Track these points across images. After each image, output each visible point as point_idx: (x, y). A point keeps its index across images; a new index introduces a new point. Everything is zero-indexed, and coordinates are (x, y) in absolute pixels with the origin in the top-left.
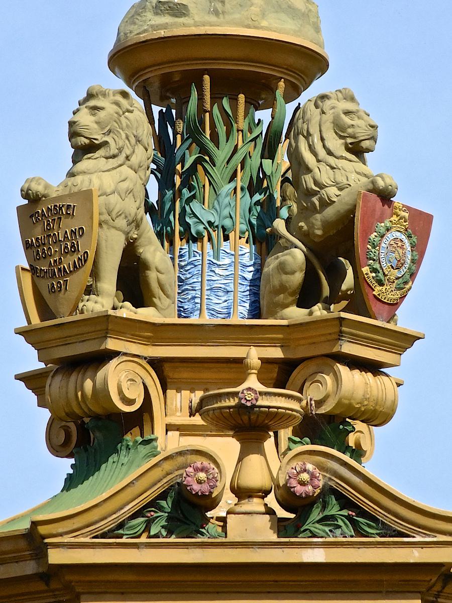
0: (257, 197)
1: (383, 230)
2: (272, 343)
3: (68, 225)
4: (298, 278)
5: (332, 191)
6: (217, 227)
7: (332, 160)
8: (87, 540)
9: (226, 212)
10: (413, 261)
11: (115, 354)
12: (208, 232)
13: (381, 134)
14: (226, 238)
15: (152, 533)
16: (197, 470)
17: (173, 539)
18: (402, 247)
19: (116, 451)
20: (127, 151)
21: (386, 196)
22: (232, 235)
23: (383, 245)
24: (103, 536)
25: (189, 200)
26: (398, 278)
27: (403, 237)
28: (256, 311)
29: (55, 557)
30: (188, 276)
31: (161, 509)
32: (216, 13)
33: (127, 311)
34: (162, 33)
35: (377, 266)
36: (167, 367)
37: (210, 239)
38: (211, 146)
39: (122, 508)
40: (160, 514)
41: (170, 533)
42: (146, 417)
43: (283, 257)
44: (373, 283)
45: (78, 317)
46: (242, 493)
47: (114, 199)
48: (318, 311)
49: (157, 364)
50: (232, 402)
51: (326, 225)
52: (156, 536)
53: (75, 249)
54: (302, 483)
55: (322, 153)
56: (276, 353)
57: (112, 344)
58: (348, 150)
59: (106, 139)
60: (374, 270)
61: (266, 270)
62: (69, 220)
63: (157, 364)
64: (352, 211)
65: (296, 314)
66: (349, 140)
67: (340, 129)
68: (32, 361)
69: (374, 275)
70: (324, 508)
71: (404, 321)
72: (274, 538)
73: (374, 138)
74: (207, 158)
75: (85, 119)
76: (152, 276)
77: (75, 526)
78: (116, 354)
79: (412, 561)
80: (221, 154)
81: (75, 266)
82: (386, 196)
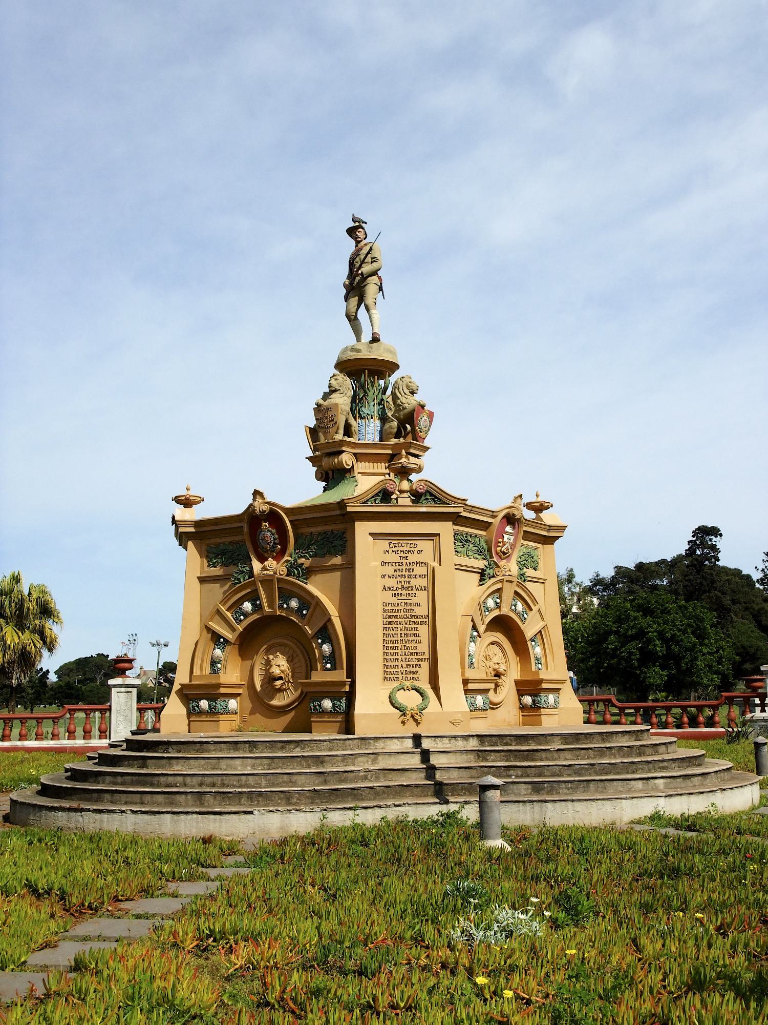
0: (381, 406)
2: (388, 449)
3: (330, 413)
4: (395, 430)
5: (406, 405)
9: (372, 410)
11: (345, 451)
16: (390, 485)
17: (382, 505)
19: (343, 480)
21: (423, 407)
24: (363, 503)
25: (361, 407)
28: (381, 440)
29: (349, 509)
31: (379, 496)
32: (370, 352)
33: (346, 439)
34: (354, 357)
36: (358, 455)
37: (368, 418)
38: (368, 391)
41: (382, 503)
42: (352, 470)
43: (390, 424)
44: (419, 432)
45: (333, 440)
46: (401, 492)
47: (343, 406)
48: (402, 440)
49: (355, 454)
50: (400, 465)
51: (404, 415)
53: (333, 421)
54: (421, 489)
55: (403, 394)
56: (390, 452)
57: (344, 449)
61: (385, 428)
62: (331, 412)
63: (355, 454)
64: (414, 410)
65: (394, 441)
67: (408, 387)
68: (199, 575)
70: (425, 496)
71: (426, 443)
72: (412, 504)
75: (333, 382)
76: (353, 428)
78: (345, 451)
80: (370, 393)
82: (423, 407)
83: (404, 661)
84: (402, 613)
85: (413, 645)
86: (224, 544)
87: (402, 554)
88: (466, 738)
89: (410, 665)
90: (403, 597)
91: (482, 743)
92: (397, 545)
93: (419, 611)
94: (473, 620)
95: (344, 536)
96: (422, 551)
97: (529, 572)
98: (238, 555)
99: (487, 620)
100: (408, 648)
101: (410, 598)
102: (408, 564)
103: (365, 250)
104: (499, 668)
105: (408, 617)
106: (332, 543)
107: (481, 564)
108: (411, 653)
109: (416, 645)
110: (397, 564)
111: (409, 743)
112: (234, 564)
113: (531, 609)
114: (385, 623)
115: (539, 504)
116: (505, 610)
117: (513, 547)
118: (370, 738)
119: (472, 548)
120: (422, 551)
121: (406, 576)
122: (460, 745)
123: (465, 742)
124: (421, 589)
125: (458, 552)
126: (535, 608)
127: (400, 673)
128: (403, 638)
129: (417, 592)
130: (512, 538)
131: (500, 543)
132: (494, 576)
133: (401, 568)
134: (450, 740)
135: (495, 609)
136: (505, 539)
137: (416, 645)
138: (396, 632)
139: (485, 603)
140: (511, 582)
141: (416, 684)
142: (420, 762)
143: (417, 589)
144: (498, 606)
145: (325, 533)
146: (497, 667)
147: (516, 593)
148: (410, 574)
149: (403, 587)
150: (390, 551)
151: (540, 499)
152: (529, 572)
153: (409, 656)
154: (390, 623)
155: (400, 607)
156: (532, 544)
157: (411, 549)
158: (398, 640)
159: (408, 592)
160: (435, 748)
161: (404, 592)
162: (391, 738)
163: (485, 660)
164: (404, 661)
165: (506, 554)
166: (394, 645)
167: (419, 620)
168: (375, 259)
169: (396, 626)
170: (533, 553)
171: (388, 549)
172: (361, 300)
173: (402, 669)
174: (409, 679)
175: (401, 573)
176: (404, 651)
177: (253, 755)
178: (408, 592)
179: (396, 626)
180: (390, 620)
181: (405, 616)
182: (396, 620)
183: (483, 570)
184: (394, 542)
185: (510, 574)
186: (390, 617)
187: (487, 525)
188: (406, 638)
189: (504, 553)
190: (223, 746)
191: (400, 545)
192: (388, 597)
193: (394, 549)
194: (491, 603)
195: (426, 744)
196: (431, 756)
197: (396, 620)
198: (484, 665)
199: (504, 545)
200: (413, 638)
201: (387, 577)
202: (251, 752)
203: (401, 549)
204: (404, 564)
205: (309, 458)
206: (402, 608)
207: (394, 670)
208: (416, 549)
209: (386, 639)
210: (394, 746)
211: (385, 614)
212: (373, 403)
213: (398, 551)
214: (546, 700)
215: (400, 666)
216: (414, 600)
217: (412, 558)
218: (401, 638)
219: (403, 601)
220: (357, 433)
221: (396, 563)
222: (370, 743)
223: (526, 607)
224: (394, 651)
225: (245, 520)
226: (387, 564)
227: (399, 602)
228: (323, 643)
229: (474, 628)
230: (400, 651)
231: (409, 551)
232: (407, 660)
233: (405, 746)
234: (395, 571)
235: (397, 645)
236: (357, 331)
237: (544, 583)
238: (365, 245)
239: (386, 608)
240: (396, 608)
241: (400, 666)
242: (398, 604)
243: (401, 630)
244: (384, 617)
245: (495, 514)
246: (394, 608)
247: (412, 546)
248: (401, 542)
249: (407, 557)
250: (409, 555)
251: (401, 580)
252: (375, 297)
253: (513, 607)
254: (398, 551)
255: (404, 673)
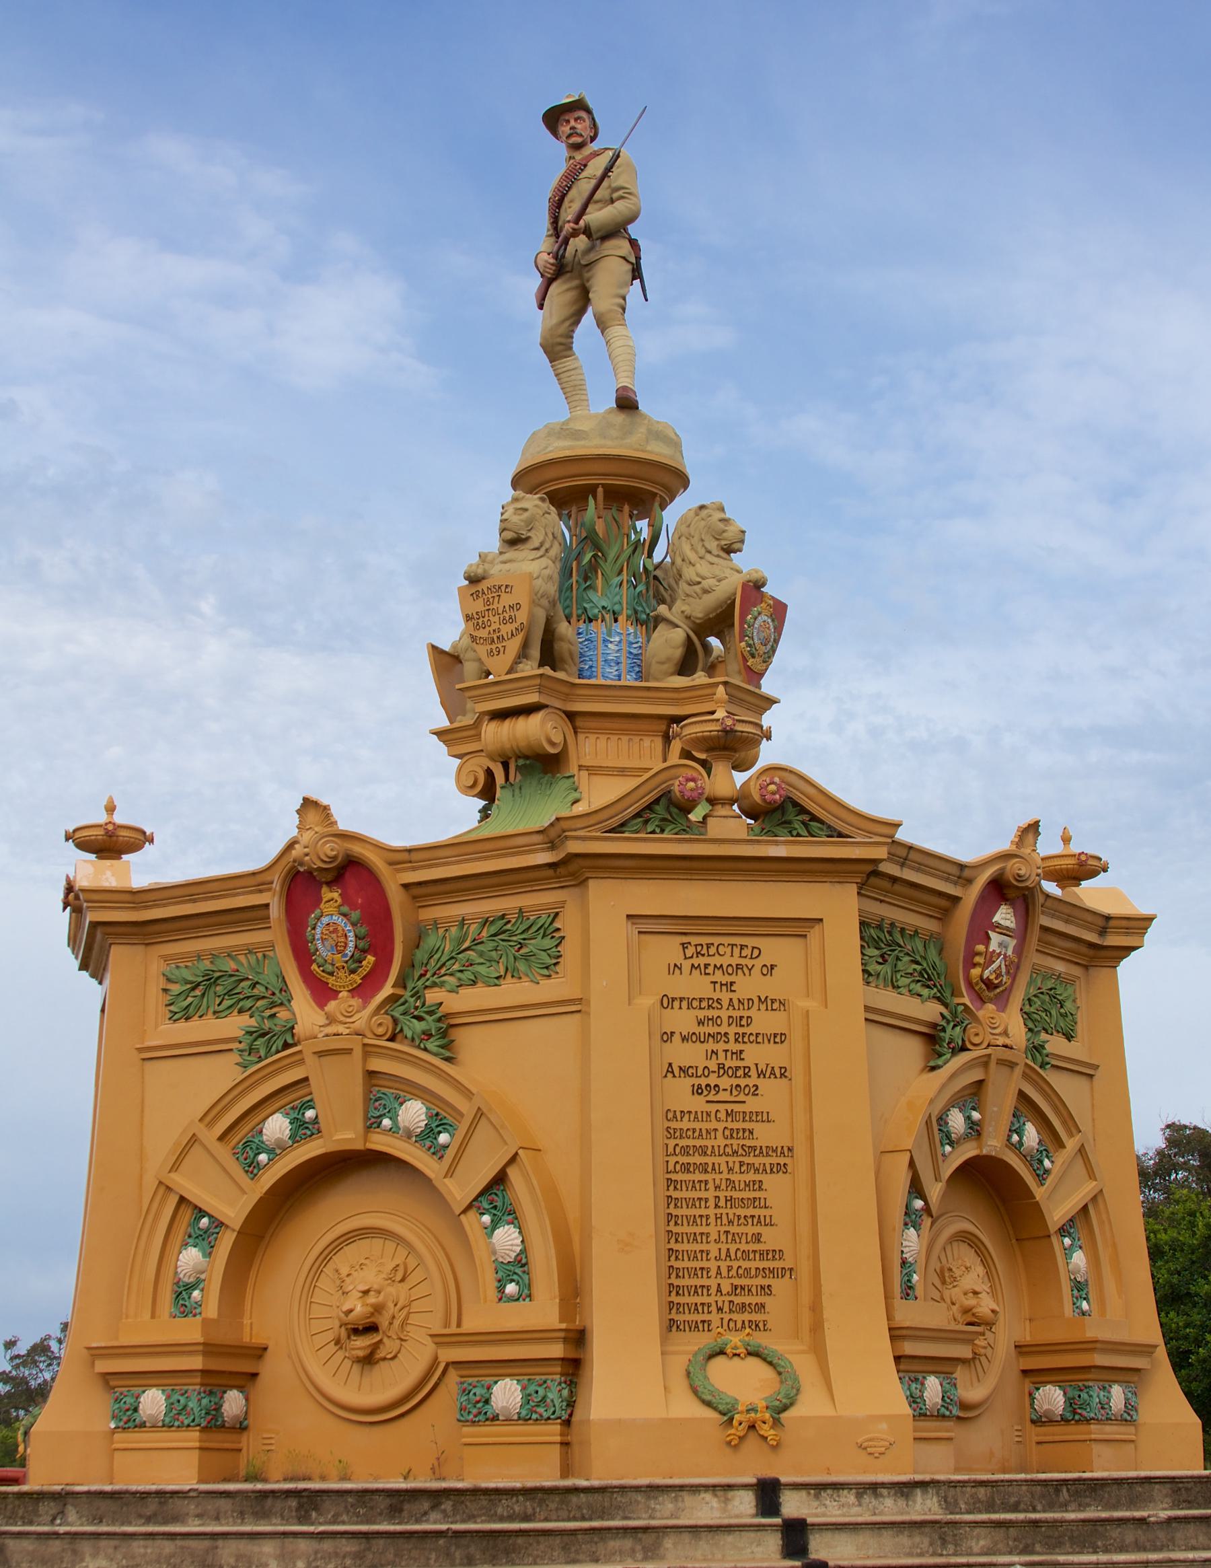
1: (756, 614)
6: (609, 611)
7: (708, 556)
8: (598, 834)
10: (774, 640)
12: (602, 614)
13: (747, 537)
14: (616, 621)
15: (649, 830)
18: (769, 628)
20: (547, 545)
22: (620, 618)
23: (756, 626)
26: (765, 653)
27: (769, 620)
30: (586, 650)
34: (568, 453)
35: (751, 642)
39: (626, 810)
40: (654, 815)
52: (653, 832)
58: (723, 549)
59: (529, 534)
60: (749, 646)
66: (723, 543)
68: (443, 722)
69: (749, 649)
73: (742, 541)
74: (600, 554)
77: (590, 823)
79: (854, 857)
81: (512, 635)
83: (724, 1273)
84: (721, 1141)
85: (751, 1230)
86: (213, 956)
87: (719, 977)
88: (905, 1489)
89: (743, 1288)
90: (724, 1096)
91: (949, 1505)
92: (704, 951)
93: (765, 1135)
94: (912, 1164)
95: (557, 925)
96: (772, 967)
97: (1055, 1044)
98: (254, 986)
99: (948, 1170)
100: (735, 1238)
101: (742, 1097)
102: (736, 1003)
103: (596, 167)
104: (978, 1305)
105: (735, 1153)
106: (522, 946)
107: (931, 1011)
108: (746, 1255)
109: (757, 1229)
110: (704, 1004)
111: (744, 1505)
112: (240, 1012)
113: (1061, 1145)
114: (671, 1167)
115: (1073, 861)
116: (993, 1145)
117: (1014, 968)
118: (637, 1489)
119: (905, 964)
120: (772, 967)
121: (732, 1037)
122: (890, 1508)
123: (901, 1503)
124: (773, 1073)
125: (870, 974)
126: (1071, 1144)
127: (713, 1308)
128: (724, 1211)
129: (760, 1082)
130: (1012, 943)
131: (979, 954)
132: (964, 1049)
133: (714, 1013)
134: (859, 1496)
135: (966, 1137)
136: (993, 946)
137: (757, 1229)
138: (703, 1195)
139: (942, 1120)
140: (1011, 1065)
141: (760, 1339)
142: (779, 1556)
143: (761, 1074)
144: (975, 1130)
145: (503, 917)
146: (971, 1301)
147: (1022, 1095)
148: (741, 1030)
149: (721, 1066)
150: (686, 965)
151: (1075, 848)
152: (1055, 1044)
153: (741, 1263)
154: (686, 1168)
155: (713, 1124)
156: (1060, 967)
157: (743, 962)
158: (708, 1217)
159: (735, 1082)
160: (817, 1515)
161: (725, 1082)
162: (695, 1489)
163: (938, 1283)
164: (724, 1273)
165: (996, 987)
166: (698, 1230)
167: (768, 1161)
168: (620, 193)
169: (703, 1177)
170: (1062, 992)
171: (679, 960)
172: (583, 299)
173: (720, 1299)
174: (739, 1325)
175: (716, 1029)
176: (724, 1247)
177: (311, 1529)
178: (735, 1082)
179: (703, 1177)
180: (685, 1159)
181: (728, 1150)
182: (703, 1160)
183: (934, 1026)
184: (694, 940)
185: (1008, 1042)
186: (685, 1151)
187: (943, 903)
188: (731, 1212)
189: (990, 985)
190: (224, 1504)
191: (712, 950)
192: (680, 1094)
193: (696, 961)
194: (957, 1121)
195: (793, 1505)
196: (811, 1537)
197: (703, 1160)
198: (937, 1296)
199: (990, 958)
200: (750, 1212)
201: (677, 1038)
202: (303, 1519)
203: (717, 960)
204: (725, 1003)
205: (440, 734)
206: (720, 1126)
207: (699, 1300)
208: (758, 963)
209: (675, 1212)
210: (706, 1510)
211: (672, 1143)
212: (617, 580)
213: (706, 966)
214: (1104, 1400)
215: (713, 1290)
216: (752, 1104)
217: (748, 987)
218: (718, 1211)
219: (722, 1107)
220: (577, 660)
221: (701, 1000)
222: (638, 1502)
223: (1047, 1140)
224: (697, 1247)
225: (277, 886)
226: (676, 1004)
227: (712, 1108)
228: (495, 1225)
229: (916, 1188)
230: (713, 1249)
231: (739, 967)
232: (733, 1272)
233: (736, 1512)
234: (700, 1023)
235: (704, 1229)
236: (572, 391)
237: (1091, 1076)
238: (596, 154)
239: (674, 1125)
240: (704, 1126)
241: (713, 1290)
242: (708, 1114)
243: (717, 1188)
244: (671, 1150)
245: (967, 873)
246: (697, 1125)
247: (745, 952)
248: (716, 940)
249: (732, 983)
250: (738, 978)
251: (715, 1047)
252: (622, 292)
253: (1015, 1138)
254: (706, 966)
255: (726, 1309)
